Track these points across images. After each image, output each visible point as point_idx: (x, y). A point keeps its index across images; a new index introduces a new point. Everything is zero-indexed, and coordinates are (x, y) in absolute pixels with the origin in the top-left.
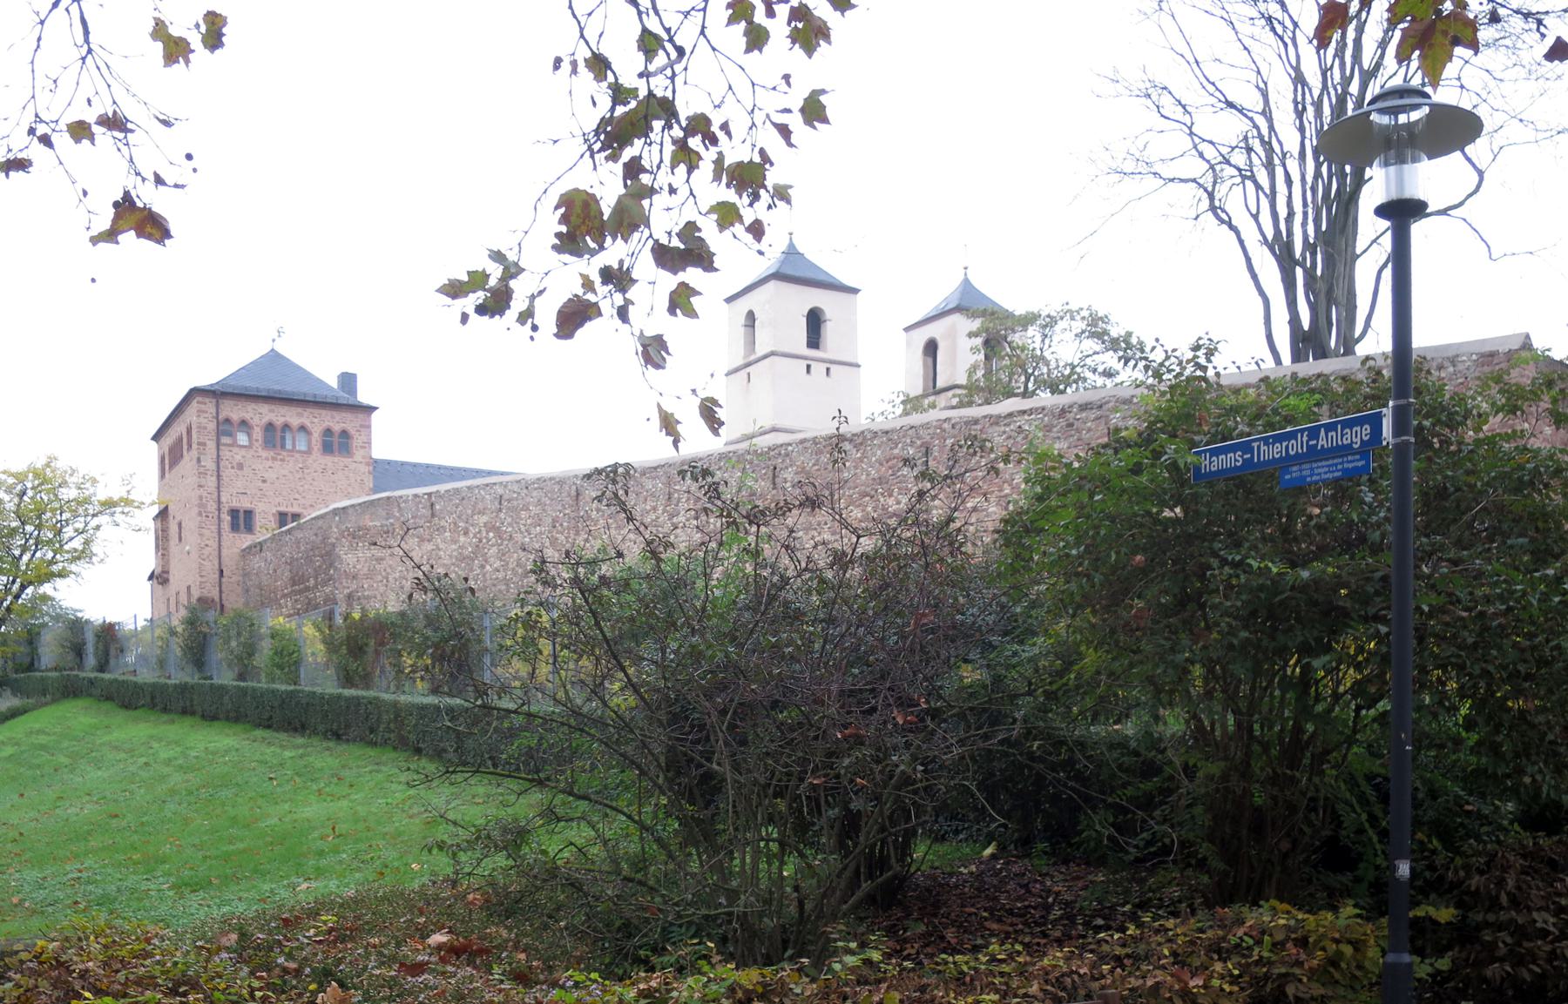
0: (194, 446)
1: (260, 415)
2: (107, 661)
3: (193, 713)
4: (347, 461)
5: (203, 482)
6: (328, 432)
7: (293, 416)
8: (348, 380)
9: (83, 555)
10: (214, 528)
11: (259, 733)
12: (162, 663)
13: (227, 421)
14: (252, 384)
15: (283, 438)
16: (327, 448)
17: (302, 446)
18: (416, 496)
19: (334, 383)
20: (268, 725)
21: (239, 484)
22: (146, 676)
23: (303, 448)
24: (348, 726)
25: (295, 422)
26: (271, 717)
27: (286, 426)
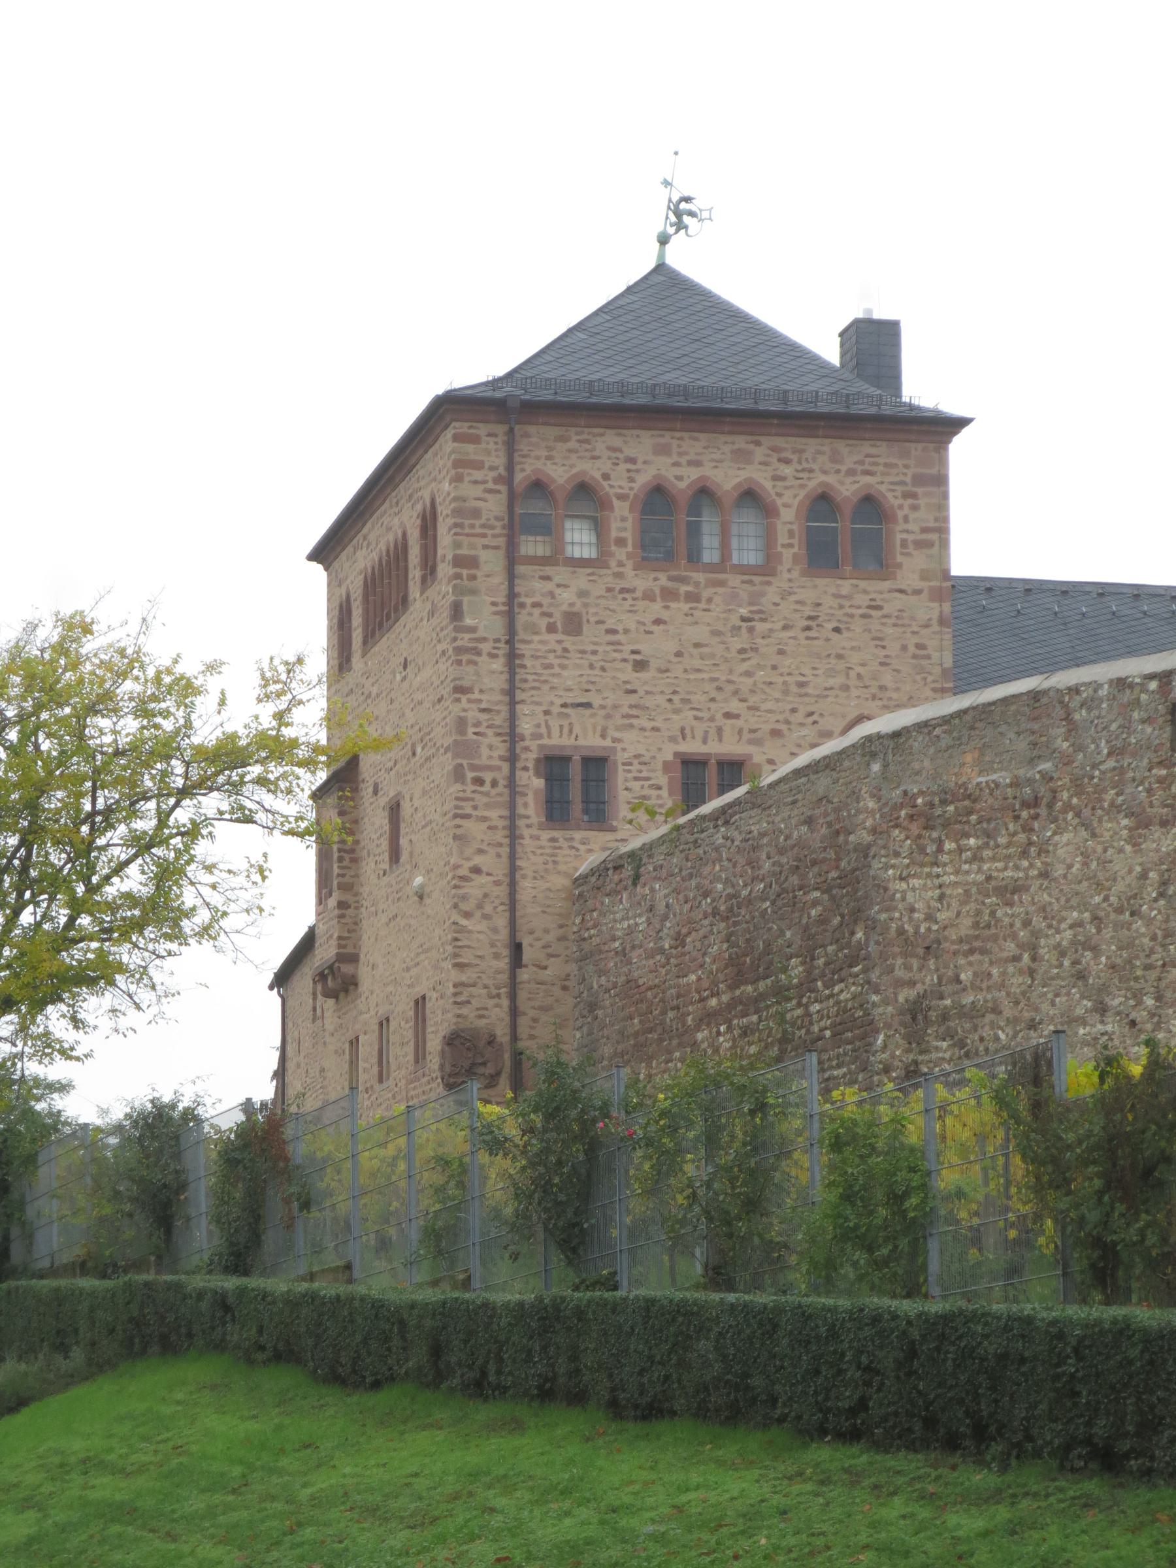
0: (444, 569)
1: (631, 464)
2: (256, 1239)
3: (578, 1398)
4: (876, 588)
5: (468, 675)
6: (823, 503)
7: (720, 463)
8: (874, 343)
9: (160, 913)
10: (496, 815)
11: (824, 1454)
12: (442, 1239)
13: (539, 487)
14: (606, 373)
15: (694, 531)
16: (821, 555)
17: (747, 553)
18: (1121, 683)
19: (831, 353)
20: (850, 1428)
21: (570, 677)
22: (392, 1281)
23: (751, 558)
24: (1149, 1426)
25: (727, 477)
26: (863, 1404)
27: (704, 493)
